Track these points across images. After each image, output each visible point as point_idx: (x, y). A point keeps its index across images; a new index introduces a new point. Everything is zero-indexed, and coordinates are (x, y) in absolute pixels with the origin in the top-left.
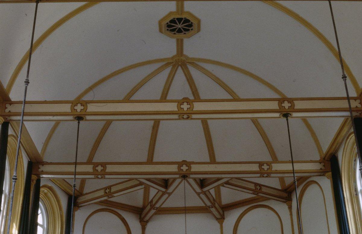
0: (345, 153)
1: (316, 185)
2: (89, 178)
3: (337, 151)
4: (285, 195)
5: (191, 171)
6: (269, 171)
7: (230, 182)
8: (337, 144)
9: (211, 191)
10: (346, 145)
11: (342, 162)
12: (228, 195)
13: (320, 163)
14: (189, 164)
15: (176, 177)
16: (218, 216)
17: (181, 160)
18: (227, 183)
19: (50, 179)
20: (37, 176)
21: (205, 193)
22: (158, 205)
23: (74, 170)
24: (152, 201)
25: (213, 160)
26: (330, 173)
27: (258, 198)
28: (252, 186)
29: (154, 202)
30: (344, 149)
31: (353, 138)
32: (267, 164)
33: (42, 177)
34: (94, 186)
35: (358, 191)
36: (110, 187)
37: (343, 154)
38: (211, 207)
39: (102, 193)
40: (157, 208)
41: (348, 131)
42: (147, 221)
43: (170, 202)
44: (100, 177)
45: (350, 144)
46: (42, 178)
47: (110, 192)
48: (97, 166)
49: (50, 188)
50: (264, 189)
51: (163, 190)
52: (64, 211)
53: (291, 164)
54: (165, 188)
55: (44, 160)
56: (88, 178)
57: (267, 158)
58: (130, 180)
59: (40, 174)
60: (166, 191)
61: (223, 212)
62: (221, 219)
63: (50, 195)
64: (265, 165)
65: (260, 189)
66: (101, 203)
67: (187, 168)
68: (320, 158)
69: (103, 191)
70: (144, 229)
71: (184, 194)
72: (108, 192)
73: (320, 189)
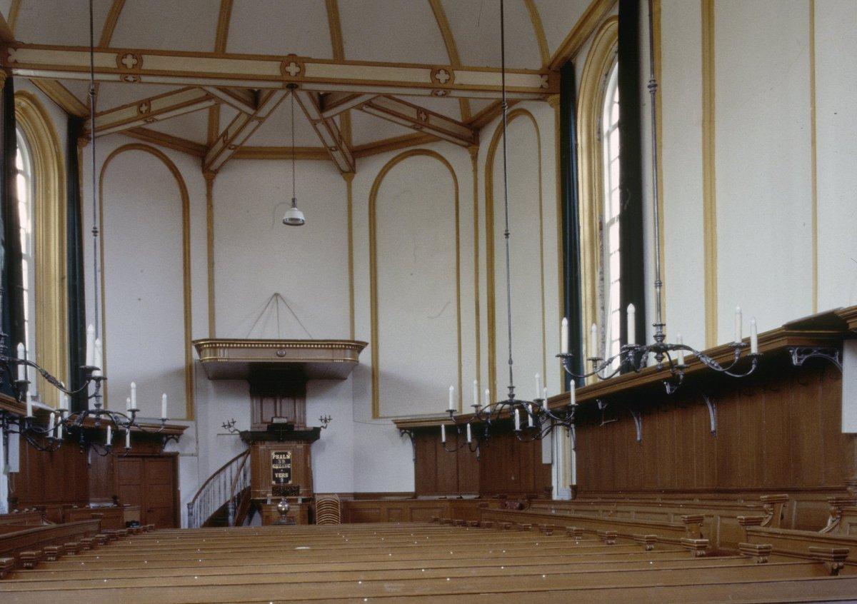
0: (590, 59)
1: (527, 118)
2: (109, 81)
3: (575, 53)
4: (468, 133)
5: (306, 76)
6: (448, 85)
7: (373, 102)
8: (577, 40)
9: (334, 118)
10: (598, 39)
11: (583, 73)
12: (364, 127)
13: (542, 75)
14: (301, 62)
15: (277, 87)
16: (345, 167)
17: (285, 54)
18: (369, 104)
19: (30, 80)
20: (6, 72)
21: (325, 122)
22: (237, 142)
23: (89, 64)
24: (226, 133)
25: (339, 57)
26: (557, 97)
27: (420, 136)
28: (412, 113)
29: (230, 135)
30: (590, 51)
31: (614, 25)
32: (446, 71)
33: (17, 75)
34: (116, 97)
35: (603, 134)
36: (148, 102)
37: (587, 60)
38: (333, 149)
39: (132, 112)
40: (236, 147)
41: (604, 15)
42: (216, 170)
43: (260, 137)
44: (130, 78)
45: (609, 33)
46: (17, 77)
47: (148, 111)
48: (125, 56)
49: (31, 98)
50: (433, 121)
51: (250, 111)
52: (62, 146)
53: (501, 74)
54: (253, 109)
55: (17, 39)
56: (103, 81)
57: (440, 57)
58: (190, 87)
59: (11, 68)
60: (255, 114)
61: (354, 160)
62: (349, 173)
63: (33, 112)
64: (442, 72)
65: (425, 120)
66: (133, 132)
67: (297, 69)
68: (544, 65)
69: (135, 108)
70: (210, 185)
71: (288, 120)
72: (146, 111)
73: (536, 134)
